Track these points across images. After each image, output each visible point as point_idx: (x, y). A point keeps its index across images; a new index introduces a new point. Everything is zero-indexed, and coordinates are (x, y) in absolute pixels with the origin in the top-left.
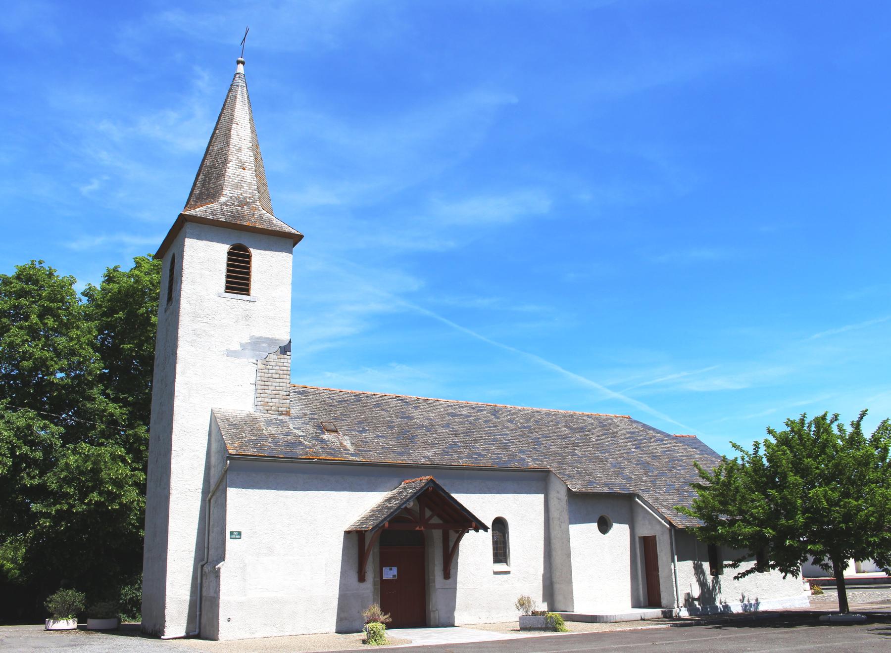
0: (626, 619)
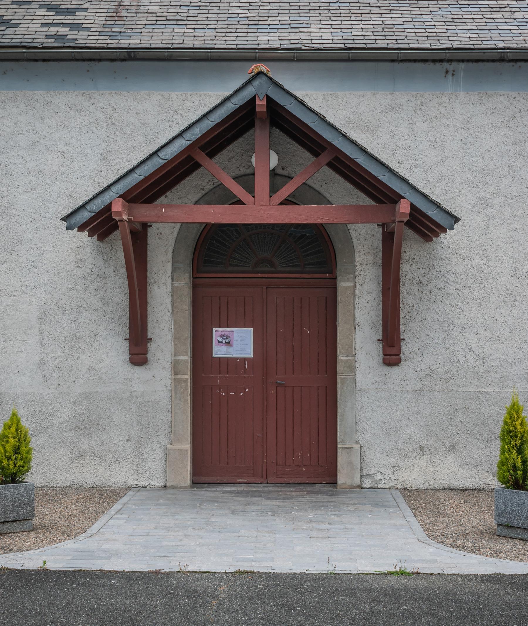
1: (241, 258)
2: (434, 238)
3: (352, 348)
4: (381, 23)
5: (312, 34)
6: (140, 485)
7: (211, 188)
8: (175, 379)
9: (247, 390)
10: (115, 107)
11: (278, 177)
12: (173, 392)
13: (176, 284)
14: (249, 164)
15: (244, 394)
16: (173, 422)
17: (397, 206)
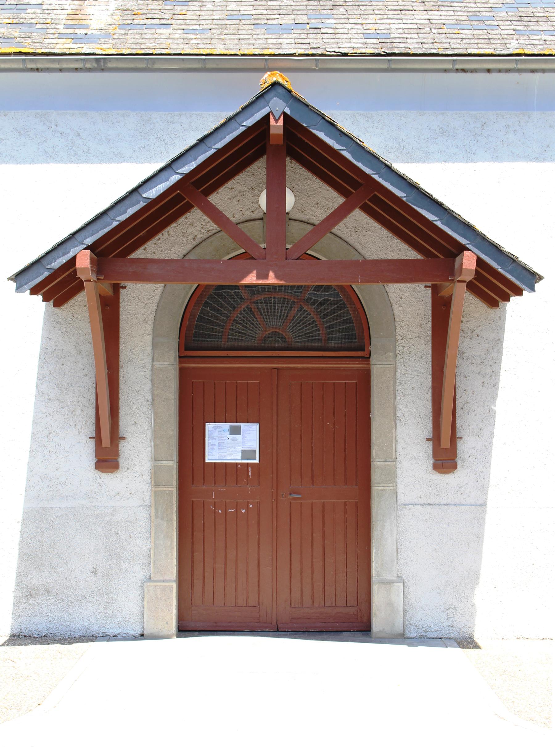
0: (332, 633)
1: (244, 330)
2: (501, 304)
3: (392, 450)
4: (427, 22)
5: (338, 36)
6: (109, 634)
7: (205, 237)
8: (155, 492)
9: (251, 506)
10: (79, 131)
11: (294, 223)
12: (153, 508)
13: (157, 365)
14: (256, 206)
15: (247, 512)
16: (153, 549)
17: (458, 259)
